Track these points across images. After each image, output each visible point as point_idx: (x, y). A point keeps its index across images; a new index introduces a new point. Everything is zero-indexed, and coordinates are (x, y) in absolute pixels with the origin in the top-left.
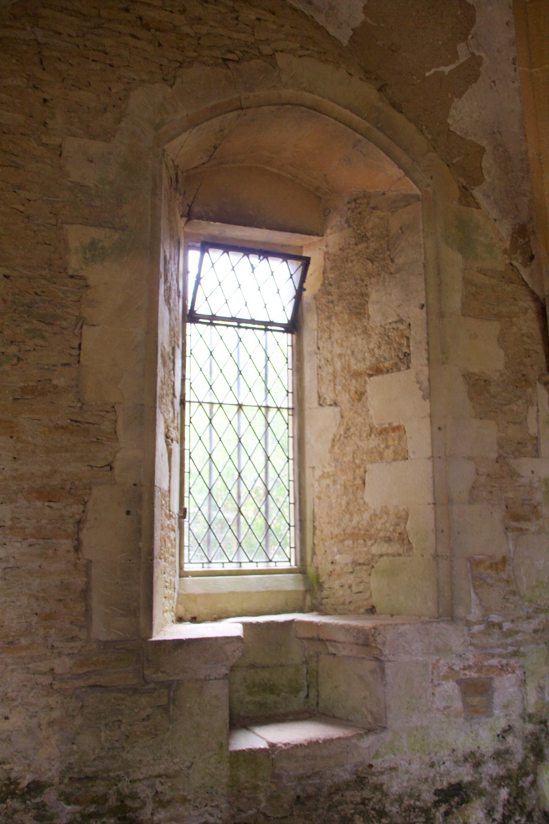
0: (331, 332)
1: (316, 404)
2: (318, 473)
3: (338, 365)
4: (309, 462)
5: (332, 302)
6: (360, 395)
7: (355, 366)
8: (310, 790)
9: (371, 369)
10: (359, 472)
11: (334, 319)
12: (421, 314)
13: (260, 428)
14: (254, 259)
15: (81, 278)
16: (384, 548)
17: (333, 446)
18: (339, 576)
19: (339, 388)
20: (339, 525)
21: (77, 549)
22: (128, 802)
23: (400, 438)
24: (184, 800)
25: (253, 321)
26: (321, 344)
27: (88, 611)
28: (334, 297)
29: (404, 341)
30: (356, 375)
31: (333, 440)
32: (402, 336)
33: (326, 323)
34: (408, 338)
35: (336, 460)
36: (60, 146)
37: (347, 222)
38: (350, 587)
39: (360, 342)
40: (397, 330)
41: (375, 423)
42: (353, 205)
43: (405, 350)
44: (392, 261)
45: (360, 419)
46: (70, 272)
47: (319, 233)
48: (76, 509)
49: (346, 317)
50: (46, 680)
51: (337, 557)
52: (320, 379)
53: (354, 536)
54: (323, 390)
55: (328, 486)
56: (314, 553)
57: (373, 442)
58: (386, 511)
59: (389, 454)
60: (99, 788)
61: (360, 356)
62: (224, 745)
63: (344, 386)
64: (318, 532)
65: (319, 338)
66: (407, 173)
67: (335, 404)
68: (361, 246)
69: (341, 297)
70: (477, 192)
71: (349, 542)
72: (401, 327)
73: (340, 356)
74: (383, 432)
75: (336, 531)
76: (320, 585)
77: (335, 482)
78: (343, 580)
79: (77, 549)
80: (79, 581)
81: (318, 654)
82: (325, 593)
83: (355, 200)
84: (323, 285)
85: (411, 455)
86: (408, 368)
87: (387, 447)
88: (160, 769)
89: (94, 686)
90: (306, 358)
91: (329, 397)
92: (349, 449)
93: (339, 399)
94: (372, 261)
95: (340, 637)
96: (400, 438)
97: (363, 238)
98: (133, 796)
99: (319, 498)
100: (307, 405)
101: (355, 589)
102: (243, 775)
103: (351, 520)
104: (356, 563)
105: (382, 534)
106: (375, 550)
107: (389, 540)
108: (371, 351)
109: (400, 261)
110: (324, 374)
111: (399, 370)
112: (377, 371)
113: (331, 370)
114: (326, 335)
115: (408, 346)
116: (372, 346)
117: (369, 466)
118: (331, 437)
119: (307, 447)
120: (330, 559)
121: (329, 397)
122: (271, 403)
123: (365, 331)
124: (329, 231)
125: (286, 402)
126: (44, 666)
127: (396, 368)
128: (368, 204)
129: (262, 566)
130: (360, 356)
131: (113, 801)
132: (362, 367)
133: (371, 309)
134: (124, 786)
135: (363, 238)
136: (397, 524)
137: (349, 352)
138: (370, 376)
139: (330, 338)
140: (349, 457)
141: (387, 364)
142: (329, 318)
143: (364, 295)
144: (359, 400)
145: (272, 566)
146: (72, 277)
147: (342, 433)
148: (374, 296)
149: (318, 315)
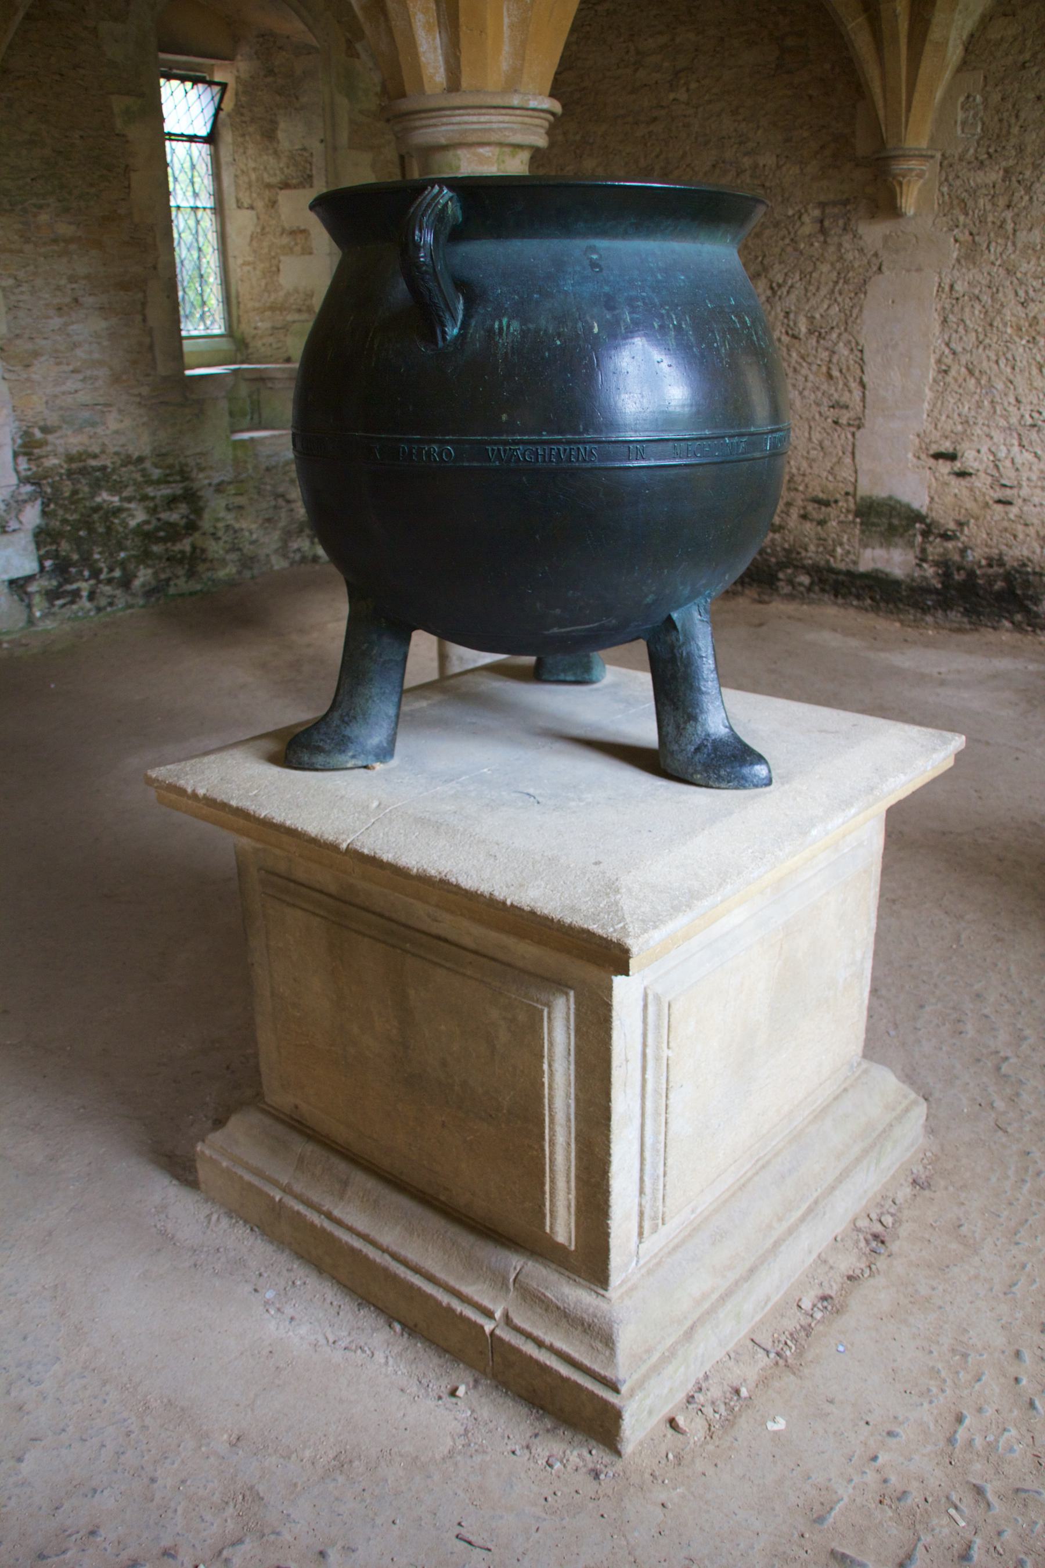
0: (246, 148)
1: (234, 206)
2: (240, 261)
3: (253, 176)
4: (231, 251)
5: (245, 122)
6: (273, 203)
7: (267, 179)
8: (273, 463)
9: (280, 183)
10: (275, 262)
11: (247, 138)
12: (320, 147)
13: (192, 223)
14: (189, 85)
15: (124, 136)
16: (296, 317)
17: (251, 240)
18: (261, 337)
19: (254, 195)
20: (259, 301)
21: (144, 320)
22: (185, 468)
23: (306, 239)
24: (211, 468)
25: (182, 135)
26: (237, 158)
27: (154, 359)
28: (247, 119)
29: (308, 166)
30: (269, 186)
31: (252, 237)
32: (306, 161)
33: (240, 139)
34: (311, 164)
35: (255, 251)
36: (95, 28)
37: (256, 53)
38: (271, 345)
39: (272, 161)
40: (302, 155)
41: (287, 226)
42: (261, 39)
43: (308, 172)
44: (297, 98)
45: (274, 222)
46: (117, 132)
47: (230, 58)
48: (140, 295)
49: (258, 137)
50: (138, 399)
51: (259, 324)
52: (237, 186)
53: (272, 308)
54: (241, 195)
55: (249, 272)
56: (239, 322)
57: (285, 240)
58: (296, 291)
59: (298, 249)
60: (170, 460)
61: (271, 172)
62: (228, 437)
63: (259, 194)
64: (242, 306)
65: (235, 152)
66: (310, 29)
67: (251, 208)
68: (270, 79)
69: (253, 120)
70: (359, 46)
71: (268, 313)
72: (306, 154)
73: (254, 169)
74: (293, 233)
75: (257, 305)
76: (246, 346)
77: (255, 269)
78: (264, 341)
79: (144, 320)
80: (147, 340)
81: (258, 390)
82: (250, 351)
83: (263, 36)
84: (236, 105)
85: (315, 251)
86: (311, 186)
87: (296, 244)
88: (198, 450)
89: (162, 403)
90: (224, 167)
91: (247, 202)
92: (265, 244)
93: (255, 204)
94: (280, 94)
95: (279, 375)
96: (306, 239)
97: (270, 72)
98: (186, 465)
99: (242, 281)
100: (226, 206)
101: (275, 346)
102: (240, 453)
103: (269, 297)
104: (274, 328)
105: (294, 307)
106: (289, 318)
107: (299, 311)
108: (281, 169)
109: (304, 100)
110: (240, 182)
111: (304, 187)
112: (286, 185)
113: (246, 179)
114: (241, 150)
115: (311, 170)
116: (281, 165)
117: (282, 258)
118: (249, 233)
119: (229, 241)
120: (253, 325)
121: (247, 202)
122: (199, 204)
123: (276, 153)
124: (239, 57)
125: (206, 201)
126: (135, 391)
127: (300, 185)
128: (275, 42)
129: (203, 333)
130: (271, 172)
131: (177, 468)
132: (274, 180)
133: (280, 135)
134: (182, 459)
135: (270, 72)
136: (305, 300)
137: (262, 167)
138: (281, 189)
139: (245, 153)
140: (266, 250)
141: (294, 181)
142: (243, 135)
143: (274, 123)
144: (273, 207)
145: (209, 332)
146: (118, 135)
147: (259, 230)
148: (282, 125)
149: (233, 131)
